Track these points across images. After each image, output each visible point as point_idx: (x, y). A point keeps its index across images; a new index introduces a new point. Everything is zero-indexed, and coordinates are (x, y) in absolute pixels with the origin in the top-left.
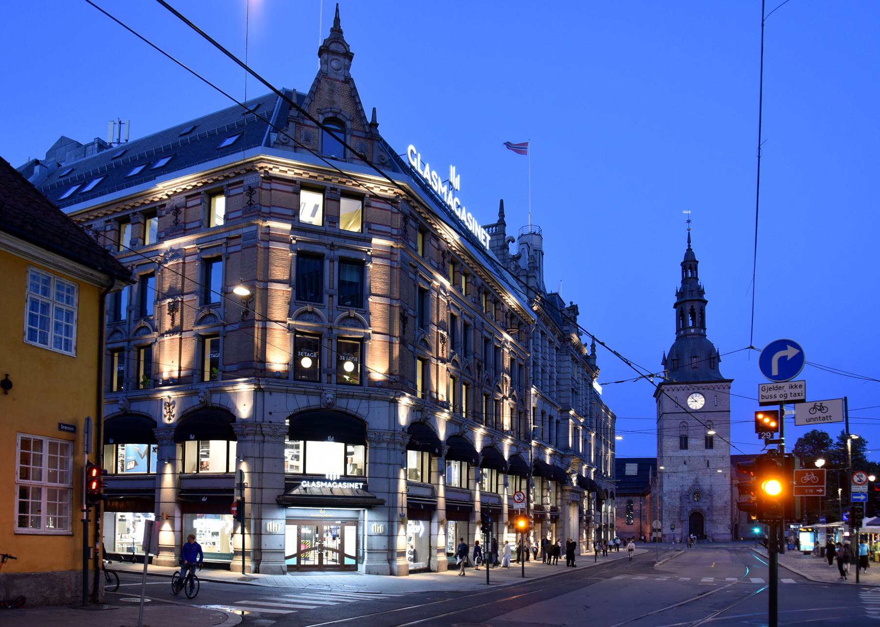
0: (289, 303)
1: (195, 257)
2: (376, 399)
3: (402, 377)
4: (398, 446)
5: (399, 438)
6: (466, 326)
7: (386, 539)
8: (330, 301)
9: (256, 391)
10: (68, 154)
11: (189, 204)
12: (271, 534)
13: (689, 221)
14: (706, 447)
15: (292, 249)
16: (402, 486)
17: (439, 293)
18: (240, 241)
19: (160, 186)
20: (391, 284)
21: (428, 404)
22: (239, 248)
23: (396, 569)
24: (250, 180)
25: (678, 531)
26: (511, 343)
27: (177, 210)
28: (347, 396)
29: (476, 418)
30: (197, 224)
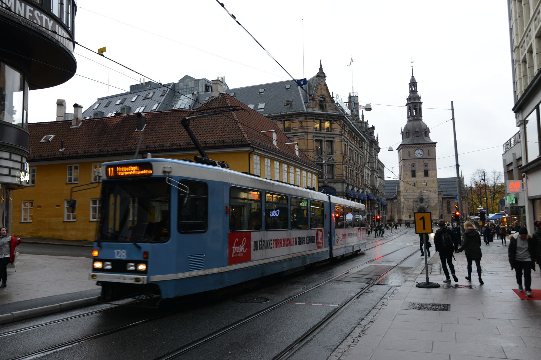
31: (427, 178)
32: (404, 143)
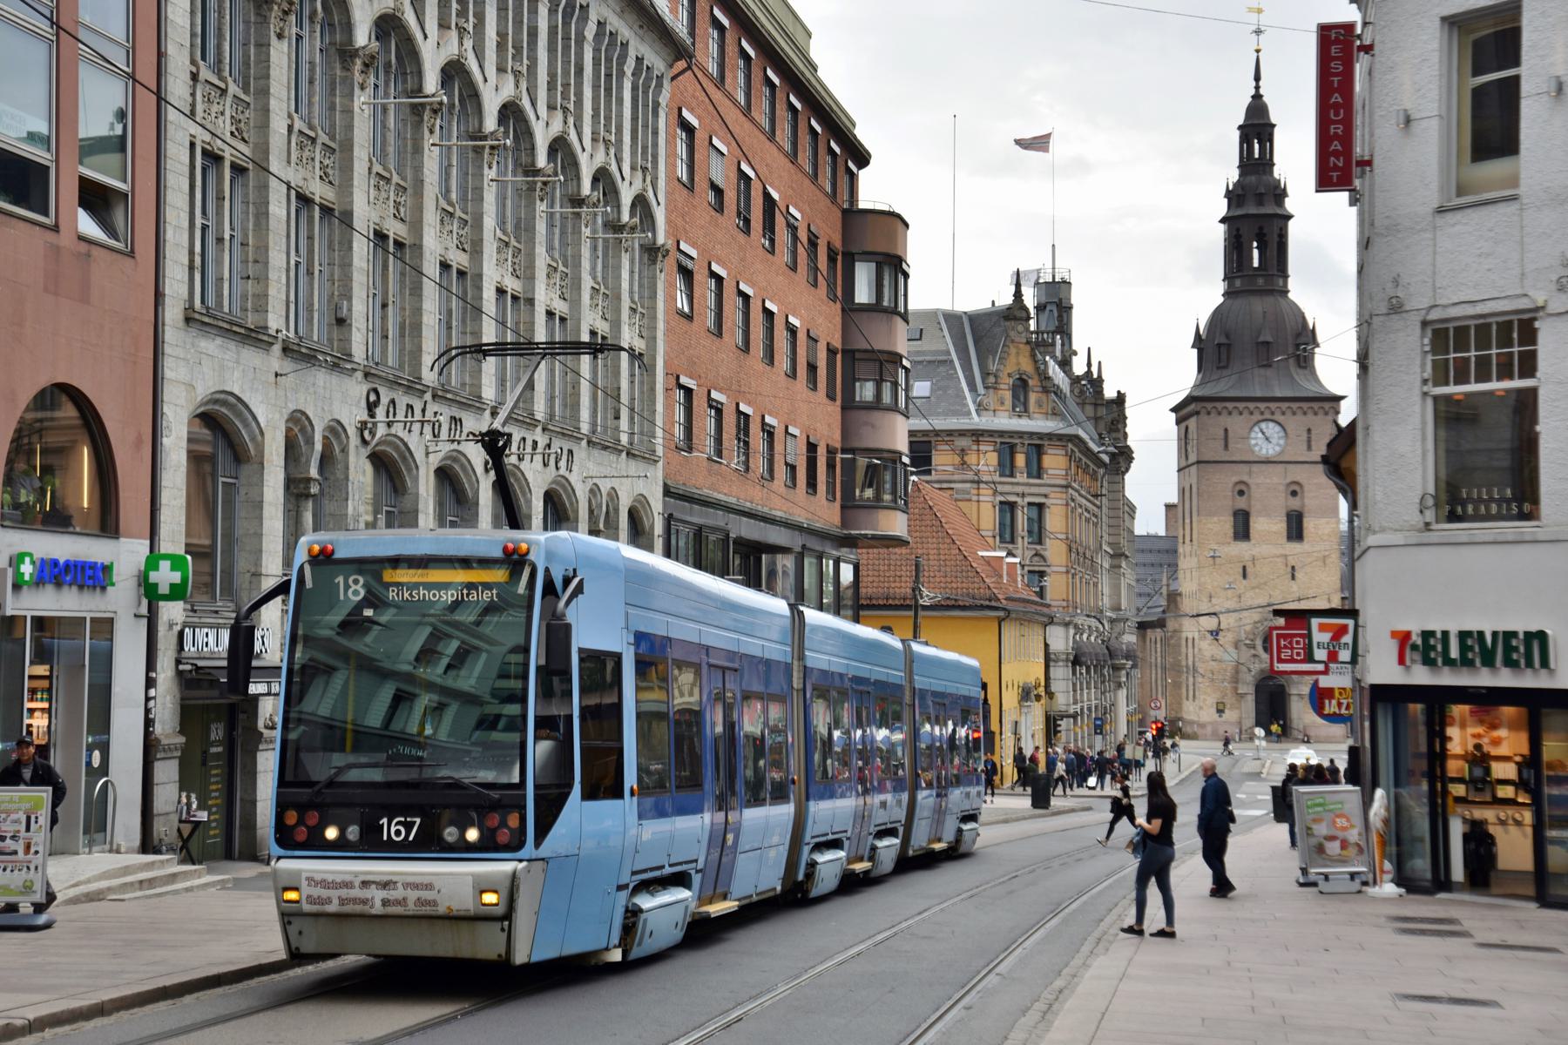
13: (1258, 32)
14: (1290, 538)
25: (1230, 715)
31: (1295, 547)
32: (1206, 392)
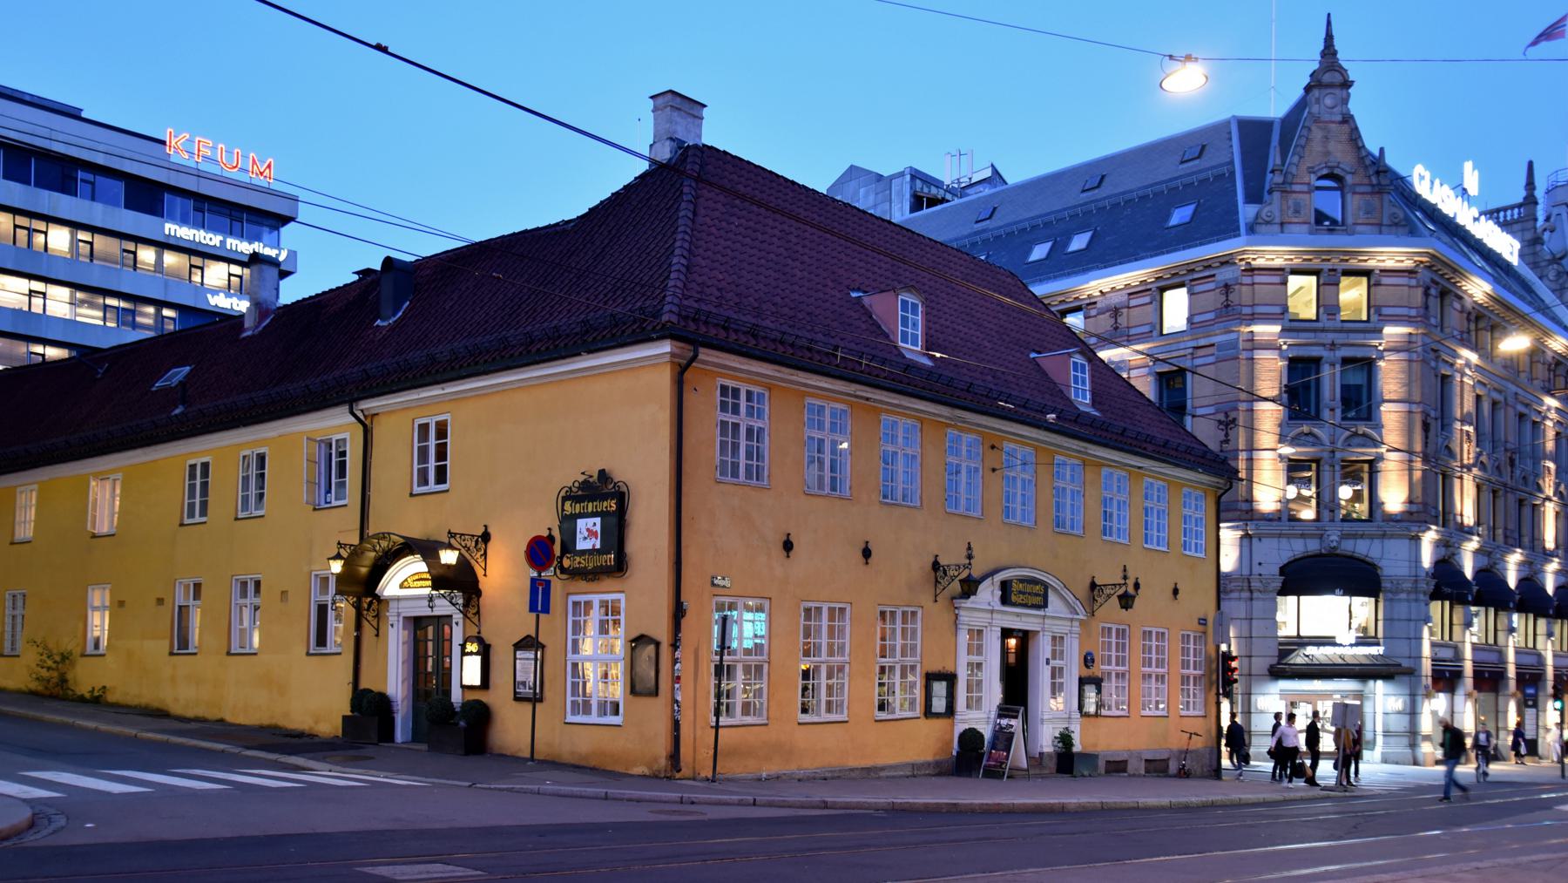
0: (1280, 425)
1: (1145, 370)
2: (1392, 537)
3: (1425, 504)
4: (1422, 597)
5: (1423, 586)
6: (1494, 404)
7: (1407, 718)
8: (1332, 414)
9: (1242, 538)
10: (862, 191)
11: (1133, 303)
12: (1262, 712)
15: (1282, 357)
16: (1426, 650)
17: (1463, 374)
18: (1210, 350)
19: (1093, 283)
20: (1409, 384)
21: (1454, 533)
22: (1211, 359)
23: (1420, 758)
24: (1225, 274)
26: (1557, 409)
27: (1115, 311)
28: (1355, 536)
29: (1513, 542)
30: (1146, 329)
